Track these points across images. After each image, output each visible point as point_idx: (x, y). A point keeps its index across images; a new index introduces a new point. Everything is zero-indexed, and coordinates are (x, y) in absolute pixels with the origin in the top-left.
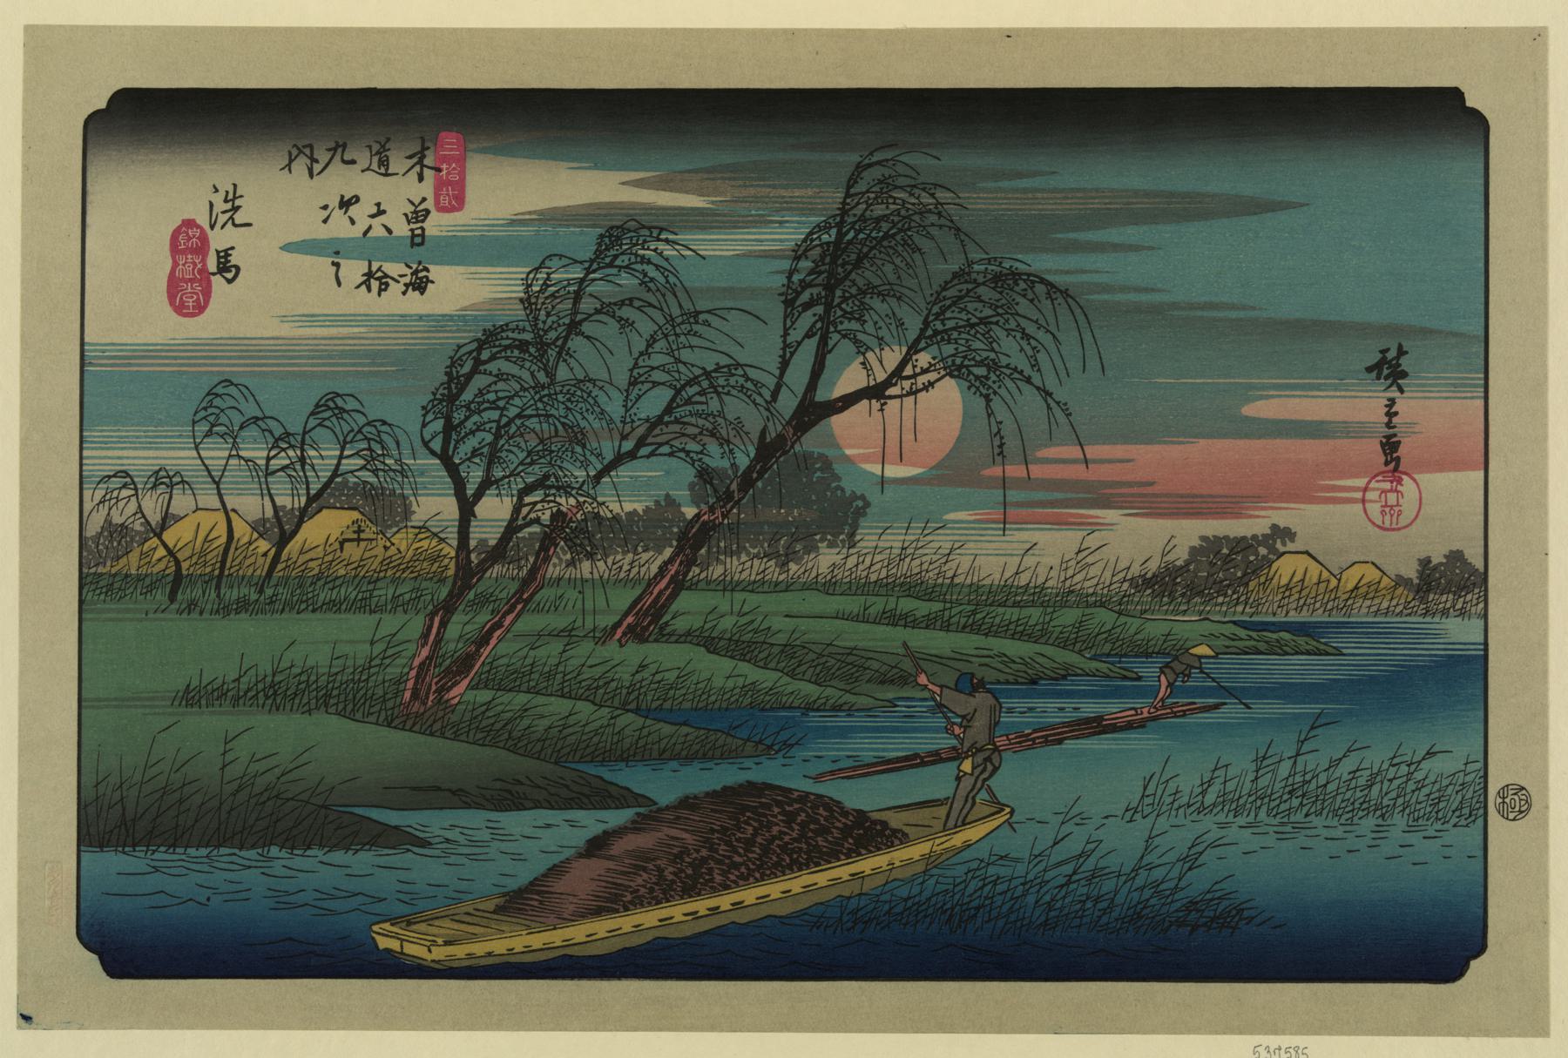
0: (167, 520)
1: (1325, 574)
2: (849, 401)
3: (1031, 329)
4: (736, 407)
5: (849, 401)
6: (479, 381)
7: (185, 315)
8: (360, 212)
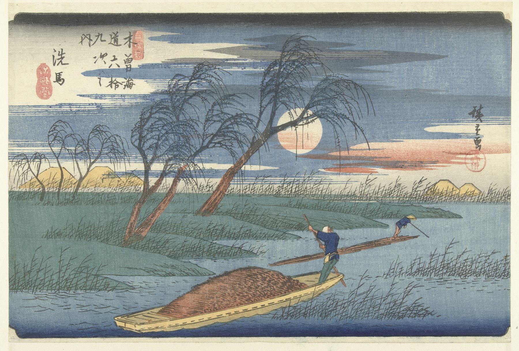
2: (284, 127)
5: (284, 127)
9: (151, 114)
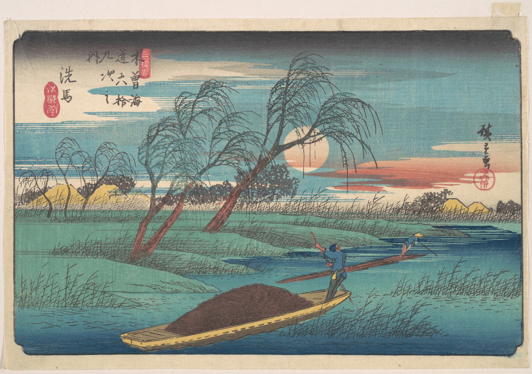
0: (46, 189)
1: (463, 207)
3: (356, 118)
4: (250, 147)
6: (158, 138)
7: (58, 112)
8: (114, 76)
9: (158, 131)
